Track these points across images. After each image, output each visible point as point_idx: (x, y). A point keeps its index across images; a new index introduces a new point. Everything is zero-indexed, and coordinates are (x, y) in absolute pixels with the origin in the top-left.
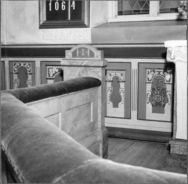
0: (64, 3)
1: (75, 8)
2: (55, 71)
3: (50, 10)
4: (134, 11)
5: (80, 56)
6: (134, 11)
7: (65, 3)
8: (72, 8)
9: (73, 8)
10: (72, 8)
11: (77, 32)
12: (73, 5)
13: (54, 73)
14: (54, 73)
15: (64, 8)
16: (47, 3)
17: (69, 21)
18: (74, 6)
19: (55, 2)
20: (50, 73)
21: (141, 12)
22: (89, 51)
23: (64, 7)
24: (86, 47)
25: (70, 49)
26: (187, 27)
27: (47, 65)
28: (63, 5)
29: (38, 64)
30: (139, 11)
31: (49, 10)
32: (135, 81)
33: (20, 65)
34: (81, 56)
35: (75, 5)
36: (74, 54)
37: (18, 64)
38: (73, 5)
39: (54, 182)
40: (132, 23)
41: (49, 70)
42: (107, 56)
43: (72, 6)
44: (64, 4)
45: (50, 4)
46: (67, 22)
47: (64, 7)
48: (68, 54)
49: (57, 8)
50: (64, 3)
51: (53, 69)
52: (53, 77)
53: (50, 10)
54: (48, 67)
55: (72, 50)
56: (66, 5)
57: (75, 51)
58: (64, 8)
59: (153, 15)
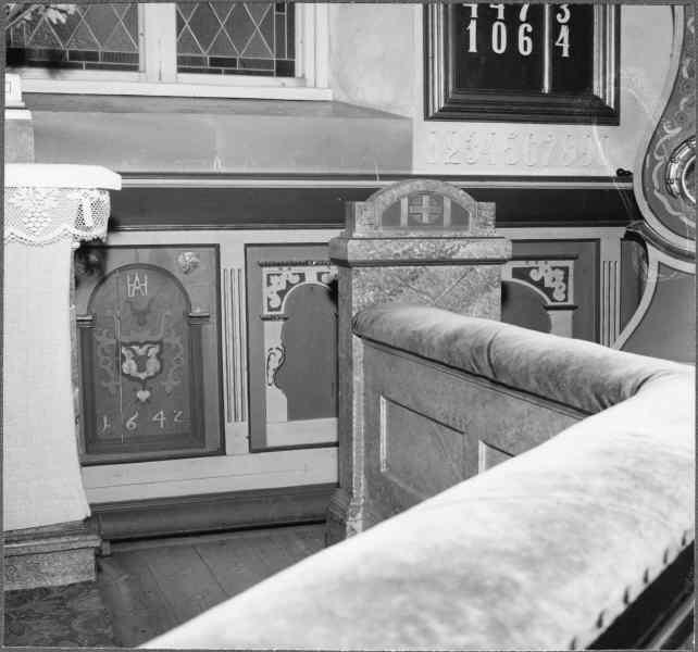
0: (526, 28)
1: (570, 54)
2: (287, 282)
3: (473, 48)
4: (212, 59)
5: (414, 223)
6: (214, 62)
7: (530, 29)
8: (556, 51)
9: (561, 53)
10: (556, 51)
11: (474, 133)
12: (562, 42)
13: (284, 287)
14: (284, 287)
15: (525, 49)
16: (462, 15)
17: (547, 95)
18: (566, 46)
19: (492, 23)
20: (564, 286)
21: (99, 63)
22: (447, 204)
23: (525, 42)
24: (440, 187)
25: (365, 195)
26: (3, 116)
27: (262, 265)
28: (522, 38)
29: (232, 259)
30: (232, 62)
31: (468, 47)
32: (236, 286)
33: (302, 277)
34: (419, 224)
35: (570, 42)
36: (391, 216)
37: (289, 274)
38: (562, 42)
39: (150, 646)
40: (280, 105)
41: (269, 279)
42: (595, 219)
43: (557, 44)
44: (526, 34)
45: (473, 27)
46: (587, 103)
47: (525, 42)
48: (365, 217)
49: (499, 46)
50: (526, 28)
51: (549, 270)
52: (566, 300)
53: (473, 48)
54: (266, 270)
55: (383, 201)
56: (536, 36)
57: (396, 206)
58: (525, 49)
59: (160, 79)
